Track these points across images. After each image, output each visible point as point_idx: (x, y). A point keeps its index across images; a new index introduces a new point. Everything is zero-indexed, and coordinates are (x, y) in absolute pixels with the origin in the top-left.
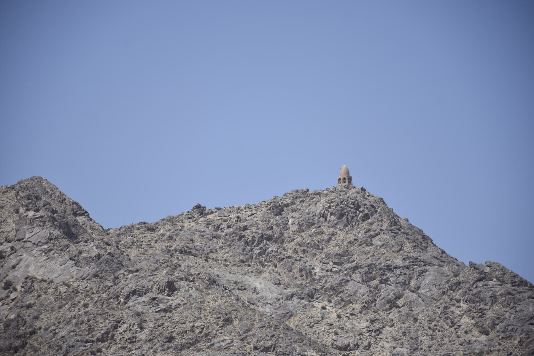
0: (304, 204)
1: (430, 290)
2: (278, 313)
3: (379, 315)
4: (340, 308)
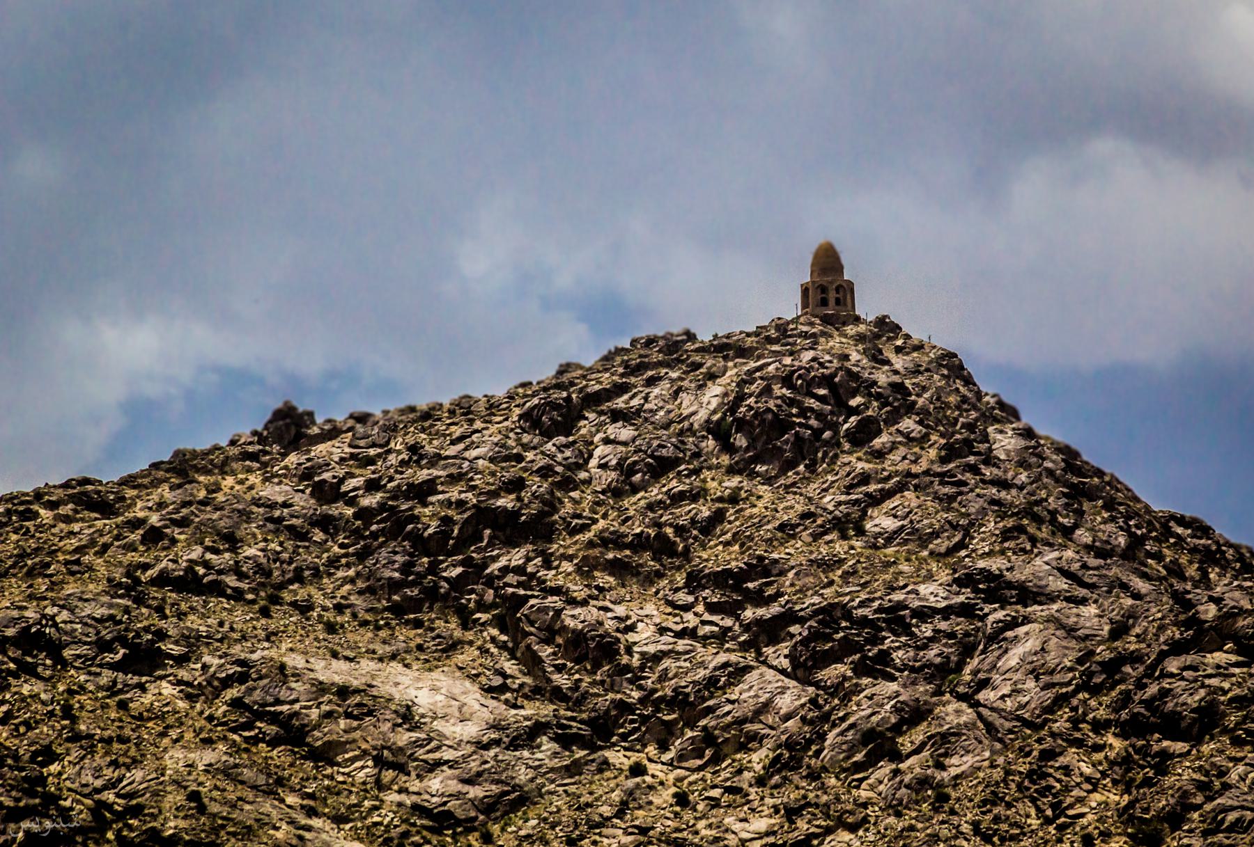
0: (656, 391)
1: (1016, 691)
2: (471, 796)
3: (823, 788)
4: (700, 769)
